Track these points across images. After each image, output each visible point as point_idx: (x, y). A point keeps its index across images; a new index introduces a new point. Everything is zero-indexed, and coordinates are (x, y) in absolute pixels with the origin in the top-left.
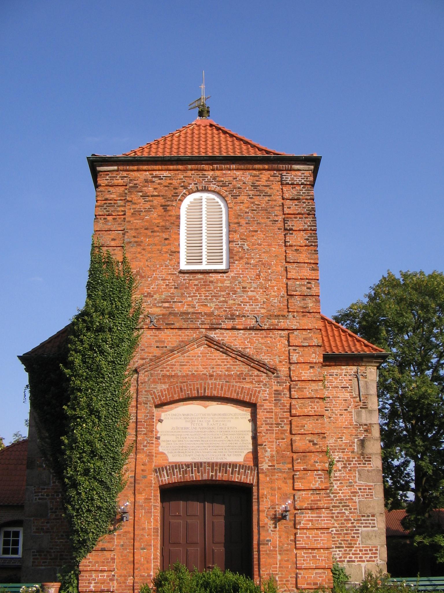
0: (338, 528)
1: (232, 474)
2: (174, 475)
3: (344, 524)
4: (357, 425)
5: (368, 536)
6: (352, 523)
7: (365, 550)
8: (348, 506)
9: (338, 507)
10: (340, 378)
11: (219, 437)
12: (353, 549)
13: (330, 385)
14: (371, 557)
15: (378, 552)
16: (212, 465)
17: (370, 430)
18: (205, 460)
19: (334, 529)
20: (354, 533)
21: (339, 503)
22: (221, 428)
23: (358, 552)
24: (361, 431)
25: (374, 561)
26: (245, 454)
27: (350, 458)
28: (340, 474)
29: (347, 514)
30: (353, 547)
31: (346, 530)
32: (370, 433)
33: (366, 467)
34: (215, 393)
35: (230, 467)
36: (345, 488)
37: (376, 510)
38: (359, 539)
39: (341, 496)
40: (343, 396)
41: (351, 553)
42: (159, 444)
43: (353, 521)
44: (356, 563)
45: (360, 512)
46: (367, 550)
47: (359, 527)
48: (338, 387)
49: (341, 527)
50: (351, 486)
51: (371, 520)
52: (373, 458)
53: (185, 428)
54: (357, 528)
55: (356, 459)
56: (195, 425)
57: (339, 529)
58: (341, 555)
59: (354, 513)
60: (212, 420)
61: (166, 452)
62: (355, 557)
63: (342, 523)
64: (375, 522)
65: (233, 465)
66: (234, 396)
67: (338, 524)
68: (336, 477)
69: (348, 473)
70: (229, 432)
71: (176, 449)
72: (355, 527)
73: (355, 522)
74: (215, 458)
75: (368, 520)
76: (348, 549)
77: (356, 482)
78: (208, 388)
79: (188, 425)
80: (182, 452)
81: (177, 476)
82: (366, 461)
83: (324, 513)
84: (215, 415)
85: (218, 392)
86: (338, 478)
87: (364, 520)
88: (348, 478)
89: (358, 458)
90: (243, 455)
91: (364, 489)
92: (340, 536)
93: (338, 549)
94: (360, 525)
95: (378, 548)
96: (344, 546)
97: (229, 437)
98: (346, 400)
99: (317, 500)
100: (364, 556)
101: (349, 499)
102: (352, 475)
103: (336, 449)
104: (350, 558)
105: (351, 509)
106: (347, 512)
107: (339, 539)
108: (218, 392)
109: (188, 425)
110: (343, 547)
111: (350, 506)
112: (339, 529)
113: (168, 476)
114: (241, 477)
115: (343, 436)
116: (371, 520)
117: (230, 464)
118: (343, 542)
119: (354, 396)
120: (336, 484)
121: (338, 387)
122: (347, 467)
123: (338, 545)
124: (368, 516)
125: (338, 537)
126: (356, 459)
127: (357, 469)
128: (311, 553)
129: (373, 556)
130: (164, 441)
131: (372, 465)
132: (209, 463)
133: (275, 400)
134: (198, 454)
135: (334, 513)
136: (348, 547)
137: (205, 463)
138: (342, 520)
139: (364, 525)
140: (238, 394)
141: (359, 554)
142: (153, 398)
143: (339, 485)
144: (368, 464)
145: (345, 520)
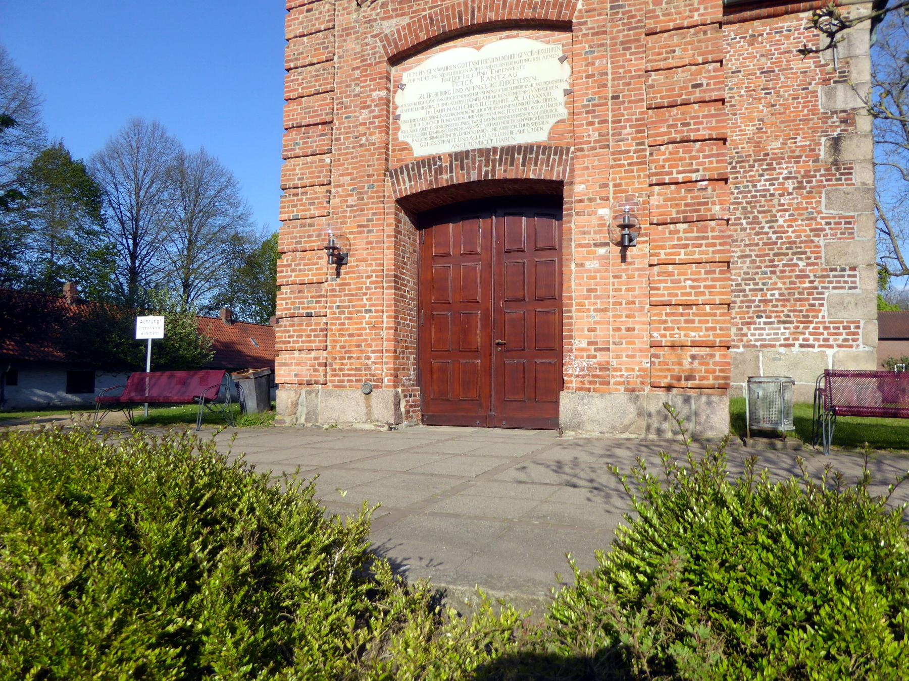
0: (784, 291)
1: (523, 165)
2: (420, 179)
3: (795, 283)
4: (827, 113)
5: (841, 304)
6: (811, 282)
7: (835, 328)
8: (805, 253)
9: (786, 255)
10: (796, 35)
11: (503, 101)
12: (812, 326)
13: (775, 50)
14: (845, 340)
15: (860, 331)
16: (486, 153)
17: (854, 119)
18: (477, 147)
19: (776, 292)
20: (814, 299)
21: (787, 248)
22: (507, 83)
23: (821, 330)
24: (834, 122)
25: (851, 347)
26: (550, 126)
27: (810, 171)
28: (790, 199)
29: (801, 267)
30: (811, 322)
31: (800, 293)
32: (853, 124)
33: (842, 185)
34: (492, 16)
35: (519, 154)
36: (800, 222)
37: (860, 258)
38: (824, 309)
39: (790, 237)
40: (800, 66)
41: (807, 332)
42: (398, 129)
43: (812, 278)
44: (816, 350)
45: (827, 263)
46: (838, 328)
47: (823, 288)
48: (790, 52)
49: (790, 289)
50: (812, 219)
51: (849, 276)
52: (857, 167)
53: (442, 93)
54: (820, 290)
55: (823, 172)
56: (460, 84)
57: (786, 292)
58: (787, 336)
59: (817, 264)
60: (489, 71)
61: (409, 140)
62: (815, 340)
63: (791, 283)
64: (857, 279)
65: (526, 148)
66: (528, 14)
67: (784, 284)
68: (783, 205)
69: (805, 198)
70: (522, 87)
71: (426, 134)
72: (816, 288)
73: (817, 280)
74: (494, 141)
75: (843, 276)
76: (802, 326)
77: (819, 212)
78: (479, 8)
79: (448, 86)
80: (436, 137)
81: (426, 179)
82: (842, 174)
83: (713, 230)
84: (495, 59)
85: (497, 13)
86: (786, 207)
87: (835, 276)
88: (805, 205)
89: (826, 170)
90: (547, 128)
91: (836, 223)
92: (788, 304)
93: (782, 326)
94: (826, 285)
95: (862, 325)
96: (795, 320)
97: (520, 97)
98: (806, 72)
99: (699, 204)
100: (832, 338)
101: (805, 242)
102: (814, 201)
103: (783, 158)
104: (804, 340)
105: (809, 258)
106: (802, 264)
107: (786, 309)
108: (497, 13)
109: (448, 86)
110: (791, 322)
111: (809, 254)
112: (786, 292)
113: (410, 181)
114: (541, 170)
115: (798, 134)
116: (849, 276)
117: (520, 147)
118: (792, 314)
119: (823, 62)
120: (781, 216)
121: (790, 52)
122: (805, 188)
123: (783, 318)
124: (843, 270)
125: (783, 306)
126: (823, 172)
127: (823, 190)
128: (682, 315)
129: (850, 337)
130: (406, 122)
131: (854, 181)
132: (480, 151)
133: (612, 8)
134: (464, 136)
135: (777, 266)
136: (802, 322)
137: (474, 150)
138: (791, 277)
139: (834, 285)
140: (535, 8)
141: (822, 334)
142: (384, 46)
143: (787, 218)
144: (846, 180)
145: (797, 277)
